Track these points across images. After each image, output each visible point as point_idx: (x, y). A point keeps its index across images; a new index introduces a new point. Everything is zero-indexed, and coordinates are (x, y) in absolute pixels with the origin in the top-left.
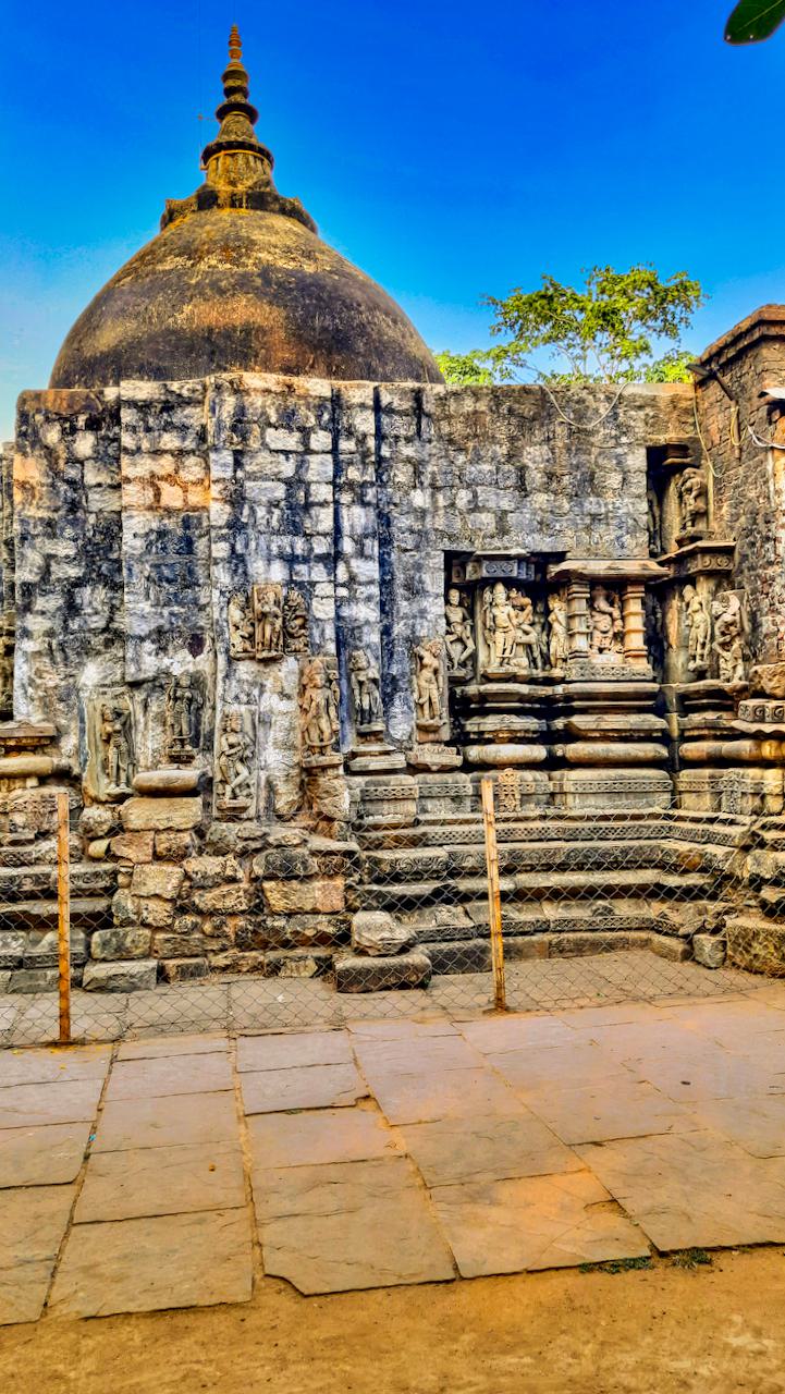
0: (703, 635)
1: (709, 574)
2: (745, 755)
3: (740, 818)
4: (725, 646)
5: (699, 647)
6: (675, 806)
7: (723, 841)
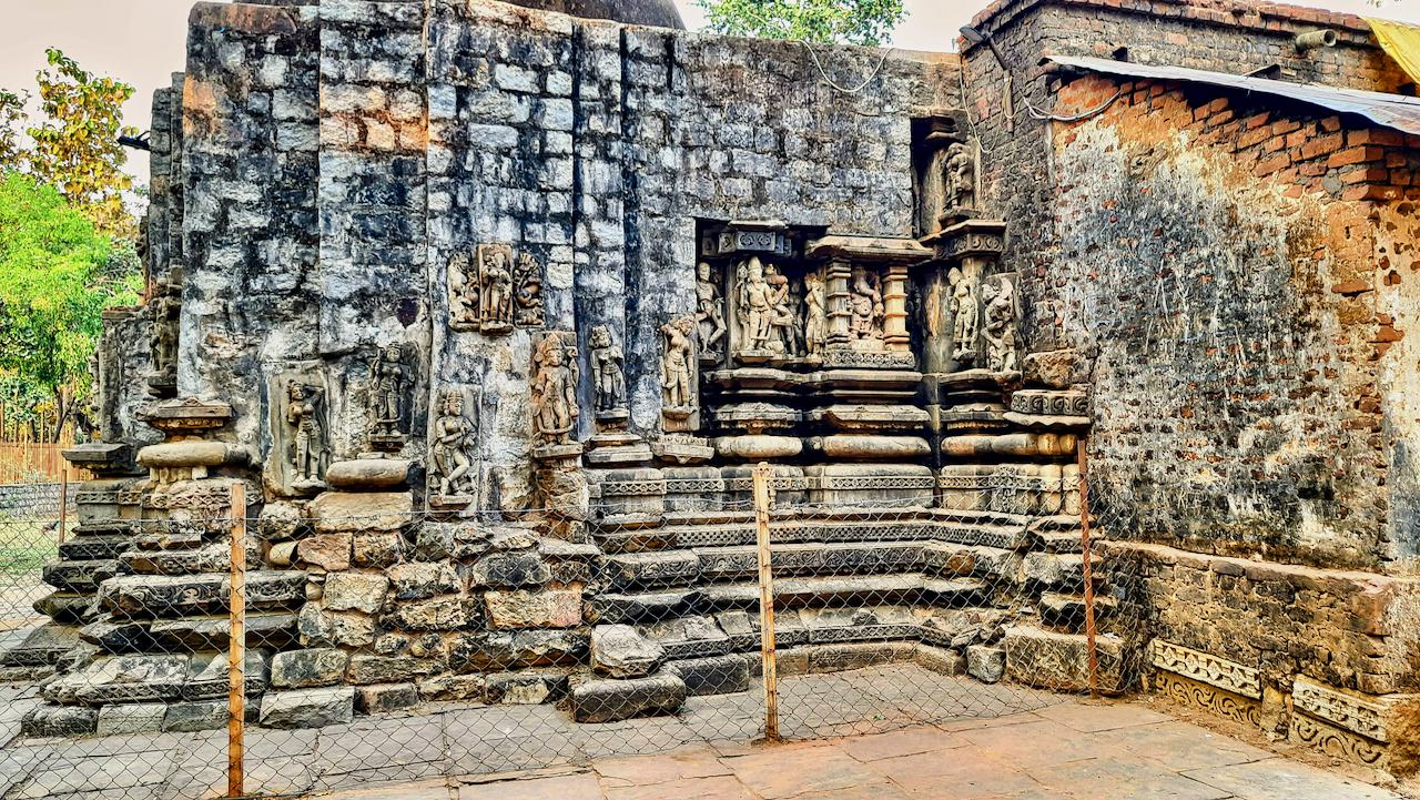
0: (970, 321)
1: (977, 256)
2: (1021, 449)
3: (1015, 518)
4: (996, 332)
5: (965, 333)
6: (935, 504)
7: (999, 542)
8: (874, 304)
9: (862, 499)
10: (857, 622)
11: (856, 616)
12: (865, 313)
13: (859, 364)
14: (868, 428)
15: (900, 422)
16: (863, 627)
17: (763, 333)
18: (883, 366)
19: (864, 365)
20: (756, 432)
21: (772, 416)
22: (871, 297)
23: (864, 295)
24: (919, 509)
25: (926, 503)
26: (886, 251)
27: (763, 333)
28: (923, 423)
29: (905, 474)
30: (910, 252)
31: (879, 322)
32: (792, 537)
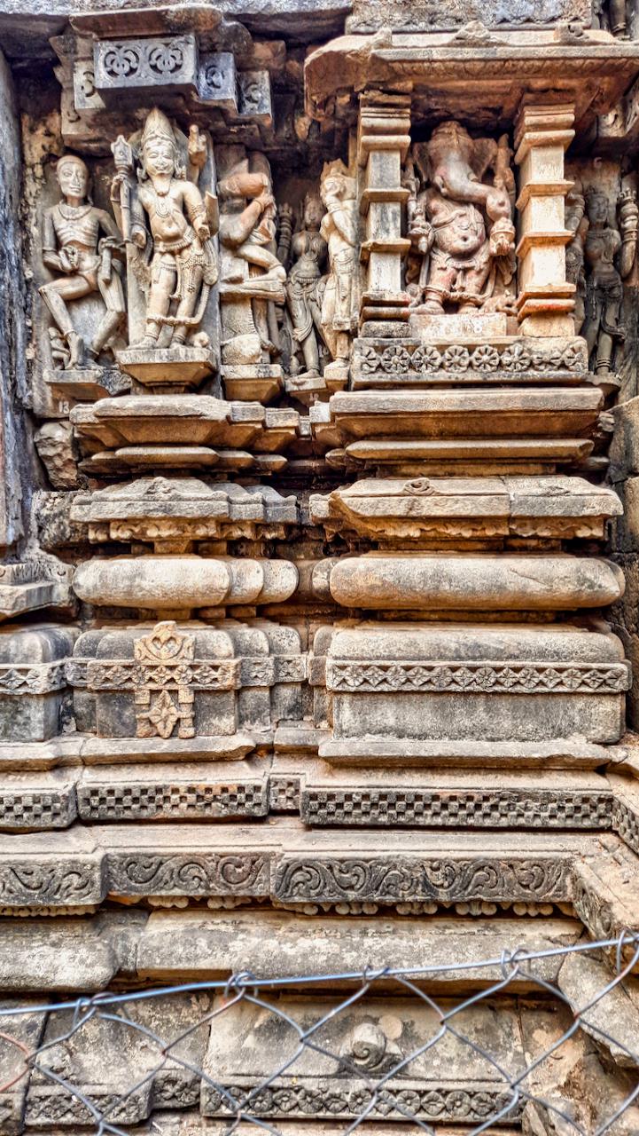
8: (488, 221)
9: (419, 716)
10: (346, 1070)
11: (344, 1049)
12: (460, 245)
13: (427, 375)
14: (437, 536)
15: (535, 521)
16: (358, 1085)
17: (185, 306)
18: (495, 377)
19: (442, 376)
20: (171, 548)
21: (191, 510)
22: (481, 206)
23: (460, 200)
24: (579, 746)
25: (598, 731)
26: (501, 52)
27: (185, 306)
28: (604, 519)
29: (542, 654)
30: (574, 51)
31: (505, 268)
32: (218, 810)
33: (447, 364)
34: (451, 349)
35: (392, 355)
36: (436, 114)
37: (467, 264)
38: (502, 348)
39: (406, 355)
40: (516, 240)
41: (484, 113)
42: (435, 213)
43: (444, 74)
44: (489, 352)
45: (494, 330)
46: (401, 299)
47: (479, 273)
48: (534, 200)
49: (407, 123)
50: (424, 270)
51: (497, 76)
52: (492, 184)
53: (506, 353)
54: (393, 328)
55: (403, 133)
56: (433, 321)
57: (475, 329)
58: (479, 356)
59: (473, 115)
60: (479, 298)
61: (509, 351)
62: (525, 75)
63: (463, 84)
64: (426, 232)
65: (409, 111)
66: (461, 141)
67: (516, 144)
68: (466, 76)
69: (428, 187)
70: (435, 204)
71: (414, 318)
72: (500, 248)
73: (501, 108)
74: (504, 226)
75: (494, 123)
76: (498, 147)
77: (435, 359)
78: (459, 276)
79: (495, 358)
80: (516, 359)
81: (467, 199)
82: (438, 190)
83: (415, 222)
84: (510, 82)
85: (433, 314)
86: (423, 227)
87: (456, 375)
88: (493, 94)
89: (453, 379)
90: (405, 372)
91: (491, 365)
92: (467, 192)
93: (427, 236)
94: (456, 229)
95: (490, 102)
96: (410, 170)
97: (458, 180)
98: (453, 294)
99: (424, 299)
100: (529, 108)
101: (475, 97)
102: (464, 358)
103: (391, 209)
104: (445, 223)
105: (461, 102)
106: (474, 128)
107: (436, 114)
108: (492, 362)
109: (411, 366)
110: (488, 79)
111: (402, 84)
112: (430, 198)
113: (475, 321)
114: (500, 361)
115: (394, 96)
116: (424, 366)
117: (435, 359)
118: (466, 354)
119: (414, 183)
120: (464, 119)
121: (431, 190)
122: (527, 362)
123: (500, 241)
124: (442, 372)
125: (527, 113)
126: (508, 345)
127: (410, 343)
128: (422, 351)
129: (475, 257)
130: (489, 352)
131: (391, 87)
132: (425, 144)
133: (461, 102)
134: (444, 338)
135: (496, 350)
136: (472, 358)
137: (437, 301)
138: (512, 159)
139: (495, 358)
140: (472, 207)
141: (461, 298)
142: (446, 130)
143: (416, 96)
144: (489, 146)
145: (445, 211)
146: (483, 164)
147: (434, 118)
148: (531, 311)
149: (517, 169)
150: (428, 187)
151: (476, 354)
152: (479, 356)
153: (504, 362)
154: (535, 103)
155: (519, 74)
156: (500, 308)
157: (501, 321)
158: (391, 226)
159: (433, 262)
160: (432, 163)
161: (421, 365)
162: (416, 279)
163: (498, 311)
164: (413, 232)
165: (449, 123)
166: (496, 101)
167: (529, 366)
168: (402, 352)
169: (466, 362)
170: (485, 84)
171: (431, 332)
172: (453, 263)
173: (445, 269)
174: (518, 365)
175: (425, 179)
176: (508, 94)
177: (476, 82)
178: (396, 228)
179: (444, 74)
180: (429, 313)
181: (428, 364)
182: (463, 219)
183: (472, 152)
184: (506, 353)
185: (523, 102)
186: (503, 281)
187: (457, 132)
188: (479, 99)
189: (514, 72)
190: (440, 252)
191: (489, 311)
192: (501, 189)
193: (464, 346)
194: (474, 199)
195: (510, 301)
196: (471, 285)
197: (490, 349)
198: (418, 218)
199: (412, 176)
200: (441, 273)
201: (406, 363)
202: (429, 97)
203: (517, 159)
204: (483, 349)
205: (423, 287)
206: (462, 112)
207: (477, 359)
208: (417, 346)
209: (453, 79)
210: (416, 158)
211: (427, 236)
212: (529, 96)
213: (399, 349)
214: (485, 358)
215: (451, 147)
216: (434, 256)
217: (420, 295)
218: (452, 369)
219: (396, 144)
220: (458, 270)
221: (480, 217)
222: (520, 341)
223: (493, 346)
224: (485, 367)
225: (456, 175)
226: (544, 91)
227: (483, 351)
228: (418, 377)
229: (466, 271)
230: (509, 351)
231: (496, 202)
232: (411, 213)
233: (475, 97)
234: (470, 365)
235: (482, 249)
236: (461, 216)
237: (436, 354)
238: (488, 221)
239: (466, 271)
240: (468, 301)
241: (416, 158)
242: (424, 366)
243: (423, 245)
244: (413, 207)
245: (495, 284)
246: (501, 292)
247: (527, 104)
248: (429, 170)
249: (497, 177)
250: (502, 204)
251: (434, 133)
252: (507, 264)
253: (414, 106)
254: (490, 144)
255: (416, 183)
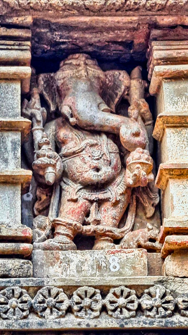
8: (123, 153)
12: (92, 176)
22: (114, 136)
23: (93, 130)
31: (142, 199)
33: (76, 308)
34: (80, 291)
35: (9, 298)
36: (63, 46)
37: (101, 196)
38: (140, 290)
39: (26, 297)
40: (155, 170)
41: (113, 47)
42: (64, 142)
43: (64, 10)
44: (125, 294)
45: (134, 268)
46: (20, 234)
47: (115, 204)
48: (168, 131)
49: (28, 55)
50: (54, 201)
51: (120, 13)
52: (126, 115)
53: (146, 296)
54: (10, 266)
55: (24, 64)
56: (62, 257)
57: (111, 267)
58: (115, 299)
59: (103, 48)
60: (117, 232)
61: (149, 294)
62: (150, 13)
63: (87, 19)
64: (53, 161)
65: (29, 43)
66: (90, 72)
67: (149, 77)
68: (88, 12)
69: (54, 116)
70: (63, 133)
71: (39, 255)
72: (137, 178)
73: (132, 42)
74: (139, 156)
75: (127, 56)
76: (131, 79)
77: (62, 302)
78: (93, 208)
79: (132, 302)
80: (158, 302)
81: (98, 129)
82: (67, 119)
83: (41, 152)
84: (135, 18)
85: (62, 249)
86: (49, 157)
87: (87, 321)
88: (119, 29)
89: (84, 326)
90: (25, 317)
91: (129, 310)
92: (97, 122)
93: (54, 166)
94: (87, 159)
95: (118, 37)
96: (36, 100)
97: (87, 110)
98: (85, 228)
99: (53, 233)
100: (158, 43)
101: (102, 32)
102: (97, 301)
103: (10, 139)
104: (74, 153)
105: (87, 36)
106: (103, 59)
107: (63, 46)
108: (129, 306)
109: (32, 310)
110: (110, 15)
111: (20, 19)
112: (59, 127)
113: (110, 258)
114: (139, 305)
115: (13, 30)
116: (48, 311)
117: (62, 302)
118: (98, 297)
119: (38, 111)
120: (95, 51)
121: (60, 120)
122: (171, 307)
123: (136, 172)
124: (71, 317)
125: (155, 47)
126: (148, 287)
127: (30, 284)
128: (46, 293)
129: (110, 188)
130: (125, 294)
131: (9, 21)
132: (52, 75)
133: (87, 36)
134: (71, 275)
135: (133, 291)
136: (106, 301)
137: (67, 235)
138: (146, 90)
139: (132, 302)
140: (104, 137)
141: (95, 232)
142: (74, 62)
143: (38, 30)
144: (121, 78)
145: (74, 141)
146: (117, 94)
147: (61, 50)
148: (172, 247)
149: (152, 101)
150: (54, 116)
151: (110, 296)
152: (115, 299)
153: (144, 306)
154: (162, 38)
155: (142, 11)
156: (142, 243)
157: (141, 258)
158: (10, 156)
159: (64, 193)
160: (59, 93)
161: (44, 309)
162: (45, 211)
163: (139, 246)
164: (37, 162)
165: (77, 55)
166: (124, 35)
167: (137, 311)
168: (21, 294)
169: (98, 306)
170: (109, 20)
171: (60, 270)
172: (86, 194)
173: (76, 201)
174: (161, 309)
175: (52, 108)
176: (135, 29)
177: (100, 18)
178: (16, 157)
179: (64, 10)
180: (58, 249)
181: (53, 308)
182: (95, 149)
183: (104, 83)
184: (146, 296)
185: (151, 38)
186: (146, 214)
187: (86, 64)
188: (105, 34)
189: (138, 9)
190: (70, 183)
191: (129, 247)
192: (136, 119)
193: (95, 287)
194: (106, 129)
195: (153, 236)
196: (106, 218)
197: (127, 290)
198: (44, 147)
199: (38, 105)
200: (72, 205)
201: (25, 306)
202: (52, 31)
203: (152, 90)
204: (118, 291)
205: (52, 219)
206: (91, 45)
207: (112, 302)
208: (40, 288)
209: (74, 15)
210: (41, 88)
211: (54, 166)
212: (155, 32)
213: (18, 290)
214: (122, 301)
215: (79, 78)
216: (64, 186)
217: (49, 227)
218: (82, 313)
219: (14, 74)
220: (92, 202)
221: (113, 147)
222: (161, 282)
223: (130, 287)
224: (121, 312)
225: (83, 104)
226: (172, 27)
227: (118, 293)
228: (41, 324)
229: (100, 202)
230: (149, 294)
231: (129, 132)
232: (36, 142)
233: (102, 32)
234: (104, 309)
235: (118, 180)
236: (92, 146)
237: (62, 296)
238: (123, 153)
239: (100, 202)
240: (104, 235)
241: (41, 88)
242: (48, 311)
243: (50, 176)
244: (39, 136)
245: (136, 216)
246: (143, 226)
247: (155, 39)
248: (57, 100)
249: (131, 107)
250: (137, 134)
251: (61, 64)
252: (148, 194)
253: (37, 39)
254: (122, 76)
255: (42, 112)
